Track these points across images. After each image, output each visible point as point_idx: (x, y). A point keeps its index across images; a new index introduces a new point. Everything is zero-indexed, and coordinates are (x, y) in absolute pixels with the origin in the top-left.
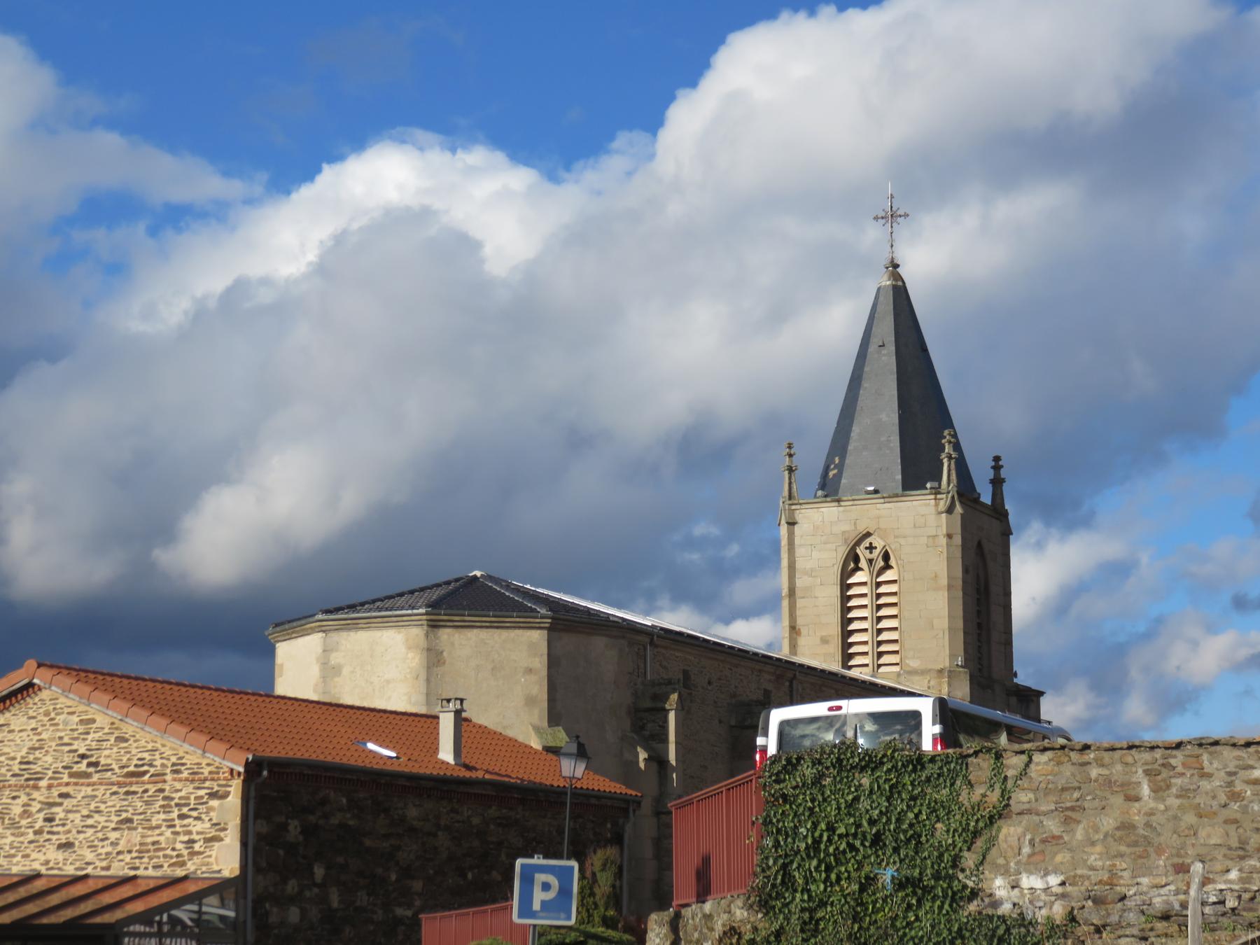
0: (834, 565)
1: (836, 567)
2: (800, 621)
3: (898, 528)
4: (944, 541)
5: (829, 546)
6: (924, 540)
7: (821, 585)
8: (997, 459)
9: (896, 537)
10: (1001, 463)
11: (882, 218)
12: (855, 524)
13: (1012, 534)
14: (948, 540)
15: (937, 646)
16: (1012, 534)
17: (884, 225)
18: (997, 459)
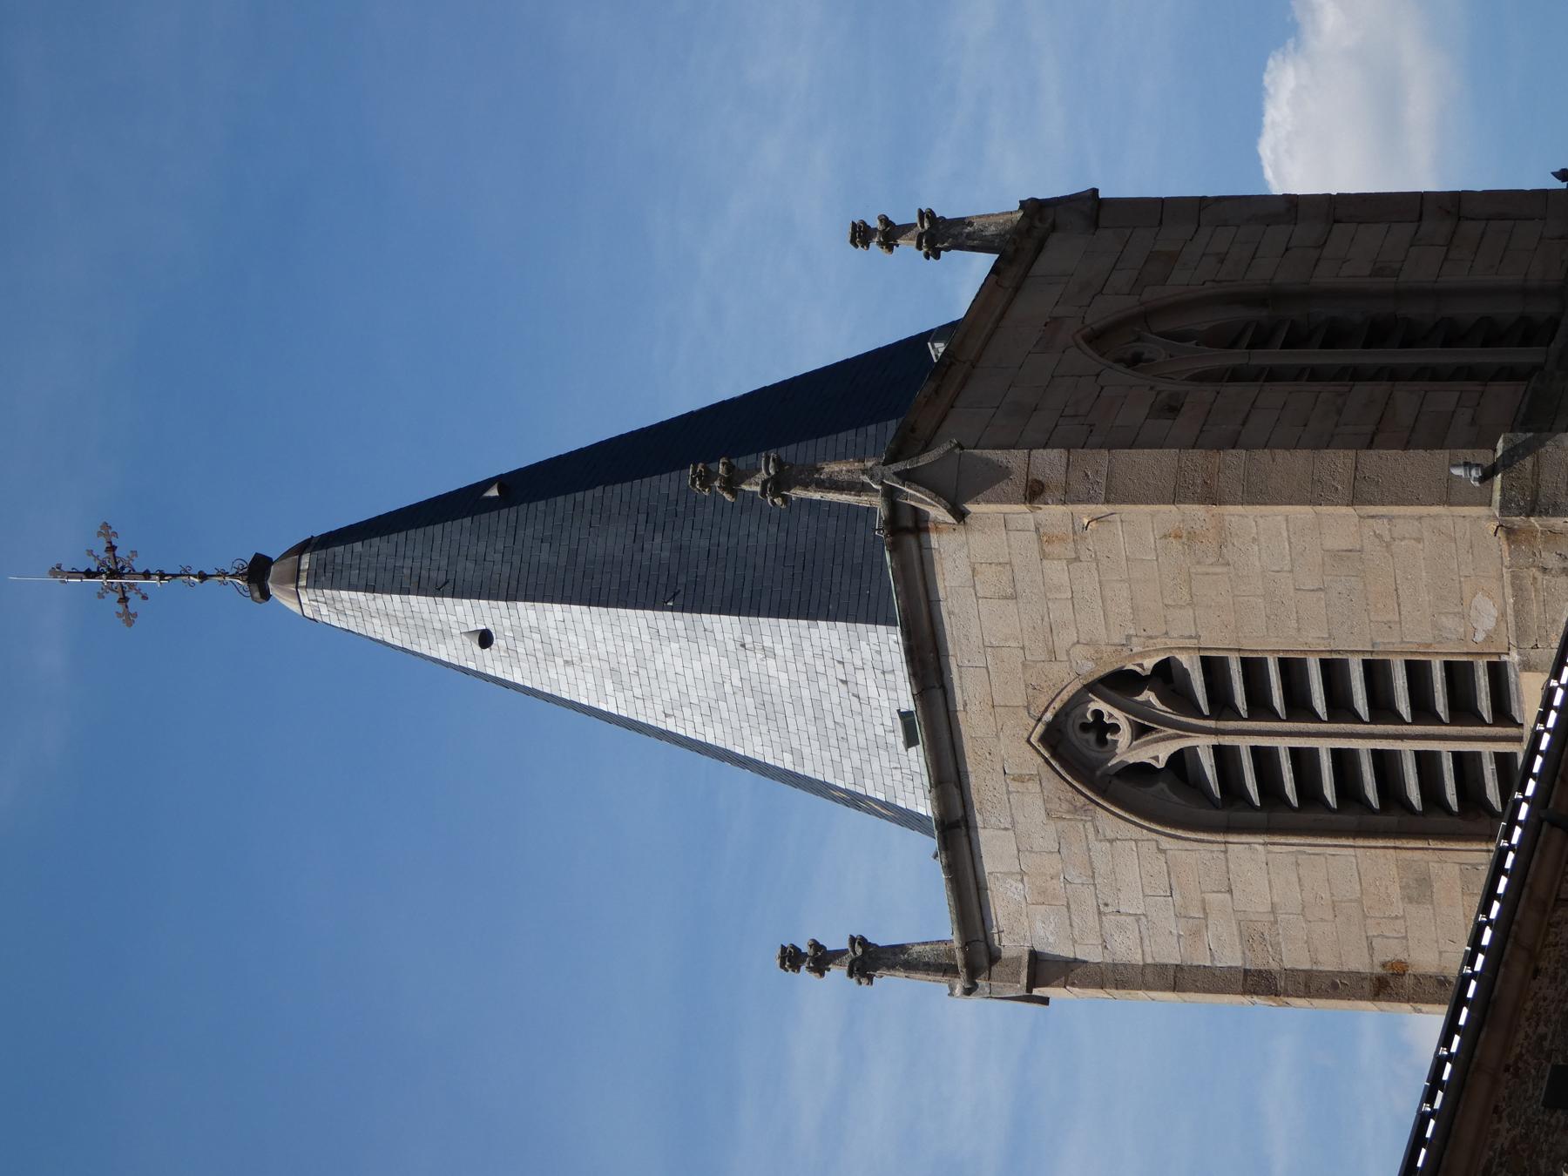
0: (1164, 851)
1: (1166, 843)
2: (1358, 962)
3: (1023, 648)
4: (1053, 513)
5: (1101, 866)
6: (1057, 571)
7: (1230, 891)
8: (861, 235)
9: (1053, 655)
10: (875, 223)
11: (124, 600)
12: (1020, 779)
13: (1095, 191)
14: (1047, 495)
15: (1419, 540)
16: (1095, 191)
17: (145, 597)
18: (861, 235)
